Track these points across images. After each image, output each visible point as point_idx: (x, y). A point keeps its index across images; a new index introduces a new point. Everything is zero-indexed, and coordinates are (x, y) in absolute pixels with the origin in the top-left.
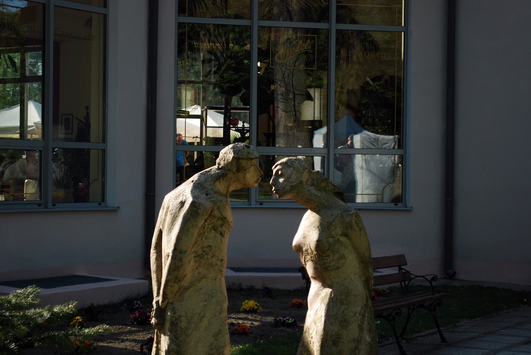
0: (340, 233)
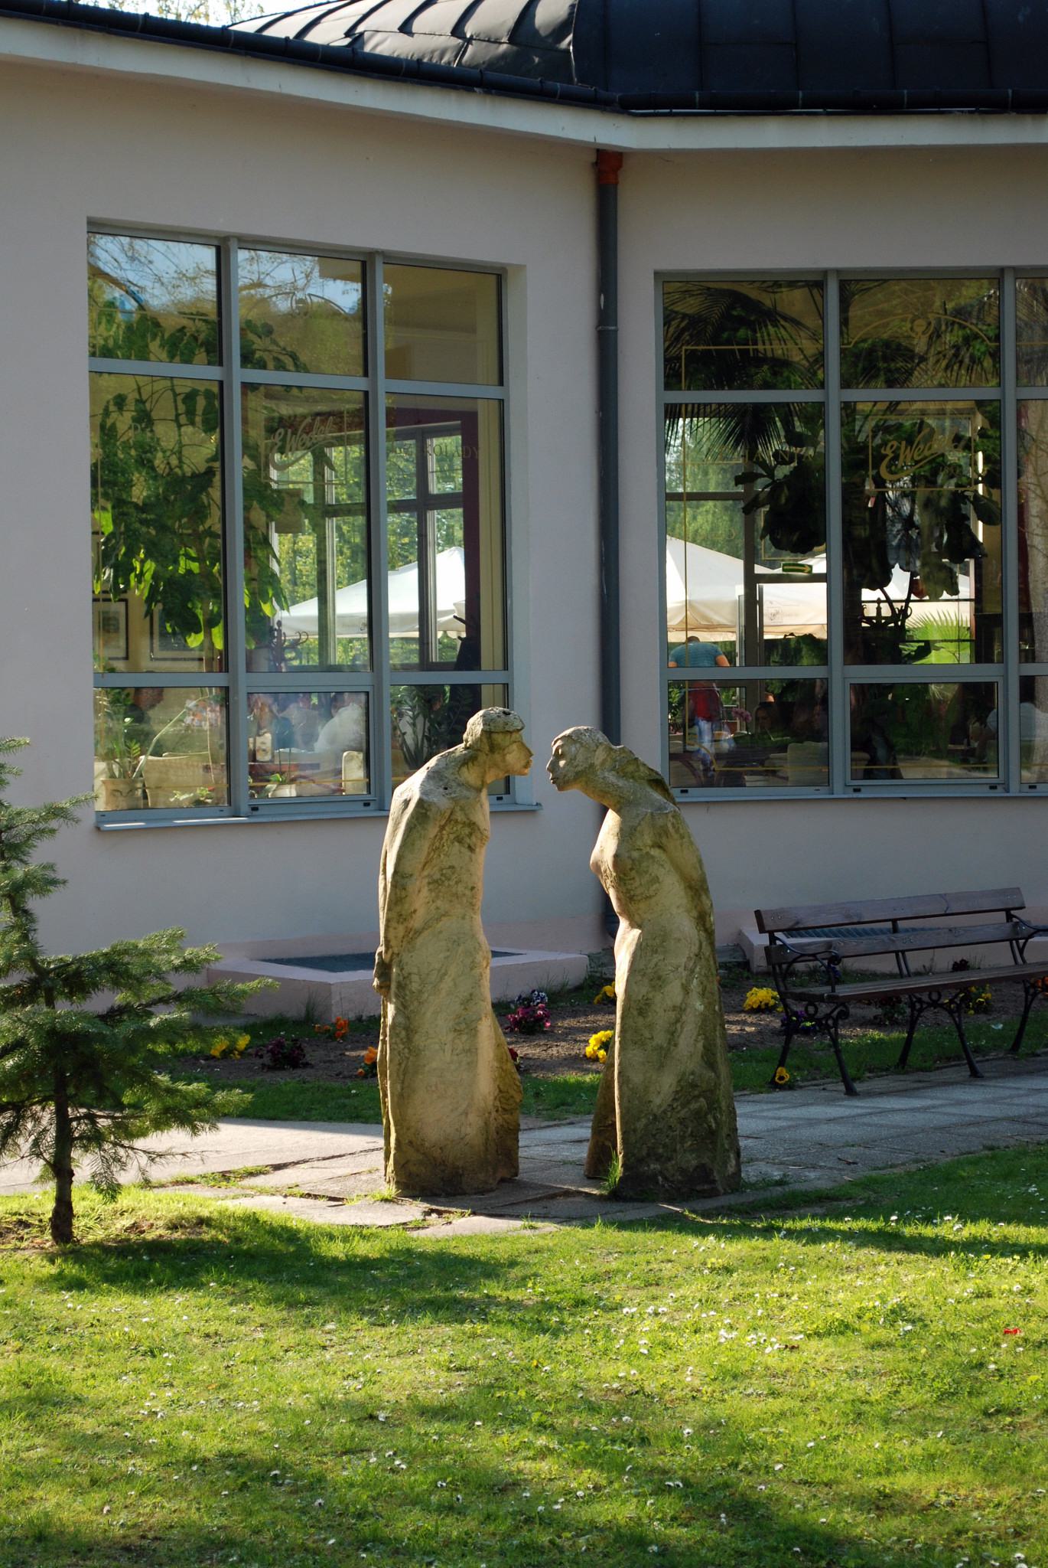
0: (649, 842)
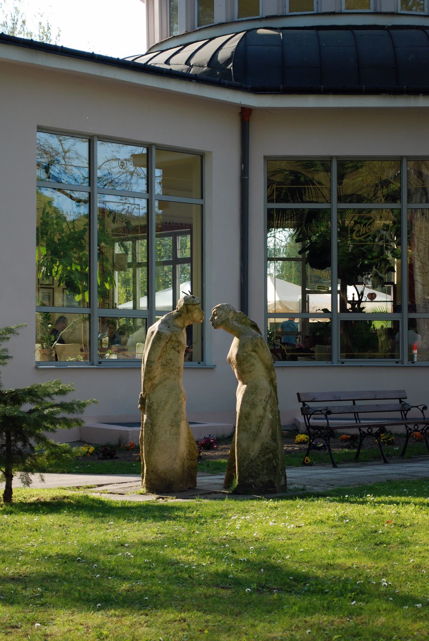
0: (251, 349)
